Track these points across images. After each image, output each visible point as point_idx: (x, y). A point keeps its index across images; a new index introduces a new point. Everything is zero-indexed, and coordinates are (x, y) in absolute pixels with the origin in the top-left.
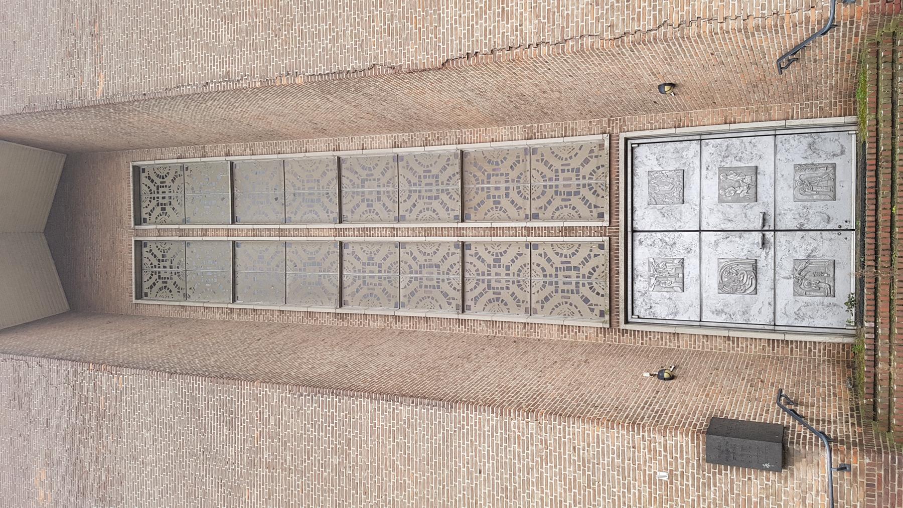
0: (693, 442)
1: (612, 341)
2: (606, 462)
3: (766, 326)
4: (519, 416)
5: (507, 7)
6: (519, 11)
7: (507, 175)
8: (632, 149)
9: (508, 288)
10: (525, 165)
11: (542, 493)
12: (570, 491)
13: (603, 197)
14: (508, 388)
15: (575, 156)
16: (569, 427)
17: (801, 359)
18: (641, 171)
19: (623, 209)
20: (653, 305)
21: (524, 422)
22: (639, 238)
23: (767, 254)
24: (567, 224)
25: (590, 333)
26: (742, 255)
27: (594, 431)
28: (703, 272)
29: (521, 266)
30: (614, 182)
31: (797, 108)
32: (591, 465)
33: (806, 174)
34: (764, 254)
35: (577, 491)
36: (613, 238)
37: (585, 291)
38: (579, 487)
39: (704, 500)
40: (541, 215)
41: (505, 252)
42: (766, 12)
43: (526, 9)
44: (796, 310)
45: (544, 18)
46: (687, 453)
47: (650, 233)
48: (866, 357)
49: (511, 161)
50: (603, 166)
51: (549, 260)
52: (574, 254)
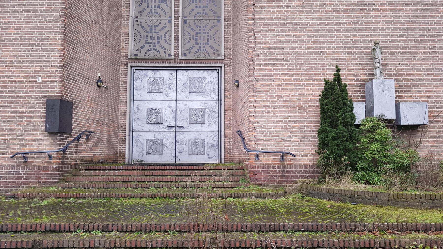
0: (57, 93)
1: (122, 59)
2: (43, 52)
3: (132, 128)
4: (62, 8)
5: (274, 4)
6: (271, 9)
7: (207, 7)
8: (216, 70)
9: (148, 7)
10: (212, 17)
11: (24, 20)
12: (26, 34)
13: (194, 56)
14: (81, 3)
15: (215, 42)
16: (58, 34)
17: (117, 142)
18: (205, 74)
19: (187, 65)
20: (141, 79)
21: (59, 11)
22: (173, 73)
23: (165, 128)
24: (180, 38)
25: (125, 49)
26: (165, 118)
27: (58, 47)
28: (157, 101)
29: (159, 14)
30: (201, 61)
31: (229, 140)
32: (40, 45)
33: (201, 144)
34: (165, 127)
35: (27, 38)
36: (173, 61)
37: (147, 47)
38: (29, 39)
39: (29, 98)
40: (186, 25)
41: (167, 5)
42: (256, 124)
43: (272, 13)
44: (140, 140)
45: (266, 23)
46: (51, 91)
47: (175, 78)
48: (107, 166)
49: (214, 9)
50: (209, 56)
51: (163, 29)
52: (166, 41)
